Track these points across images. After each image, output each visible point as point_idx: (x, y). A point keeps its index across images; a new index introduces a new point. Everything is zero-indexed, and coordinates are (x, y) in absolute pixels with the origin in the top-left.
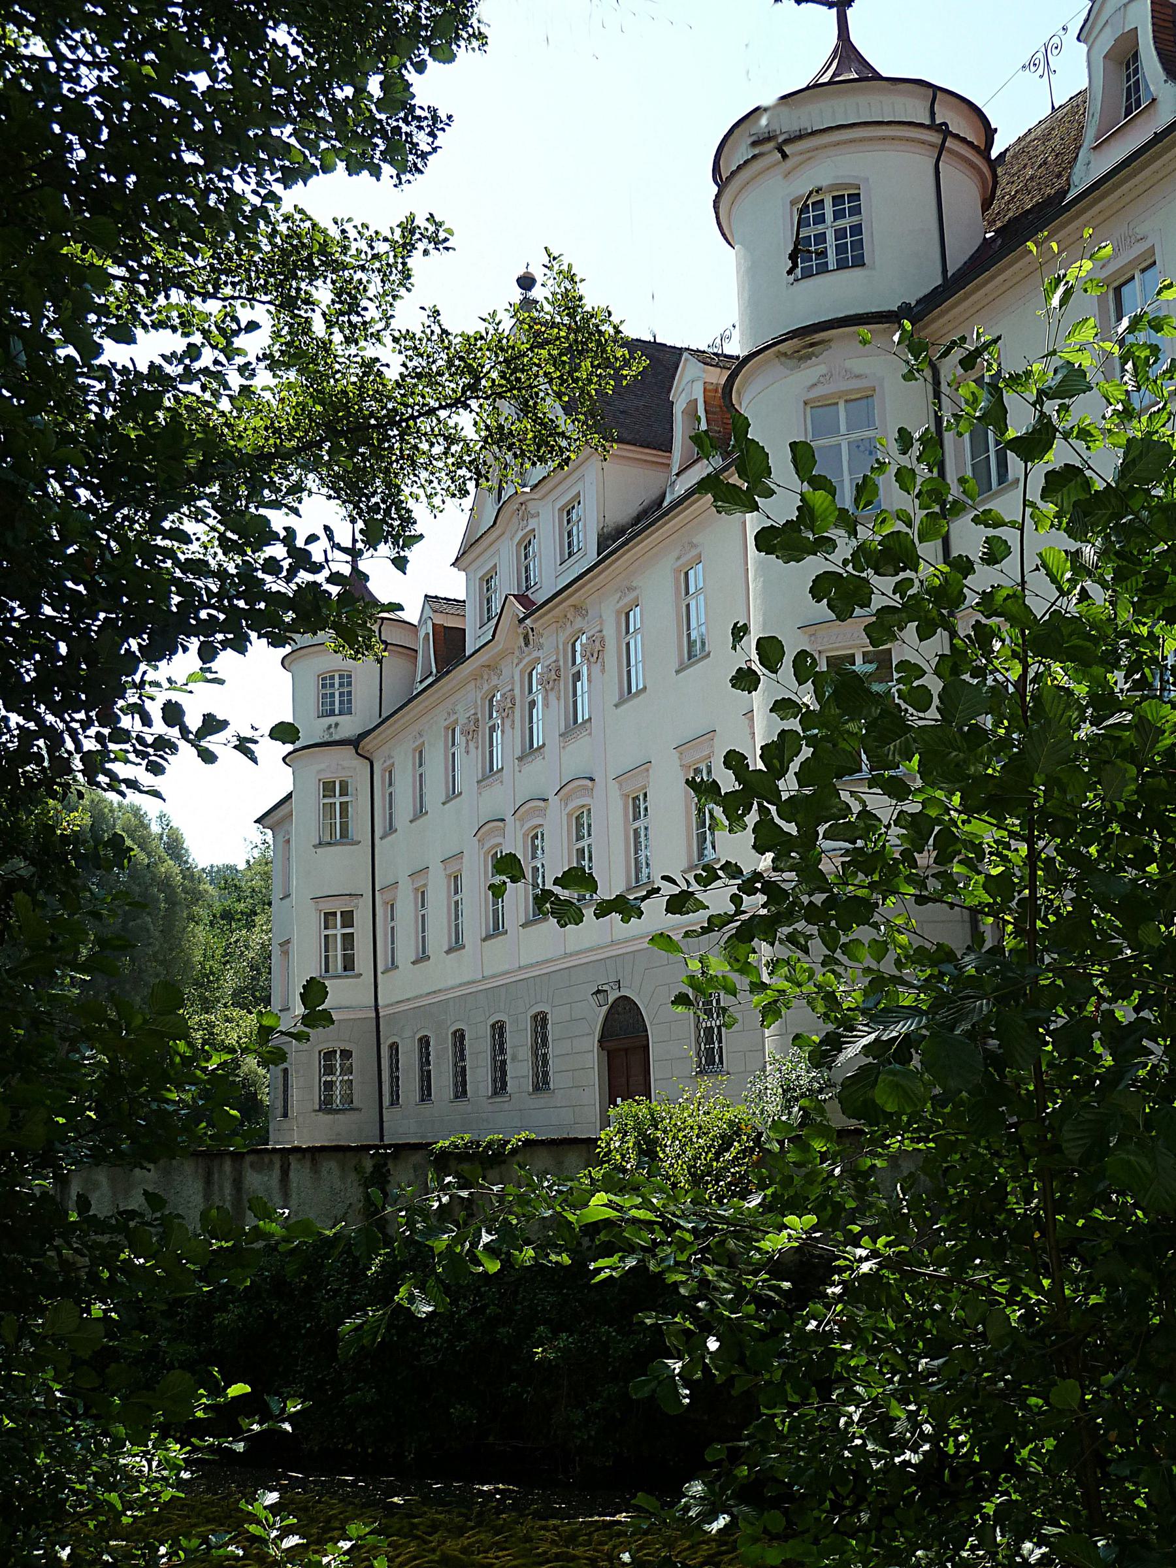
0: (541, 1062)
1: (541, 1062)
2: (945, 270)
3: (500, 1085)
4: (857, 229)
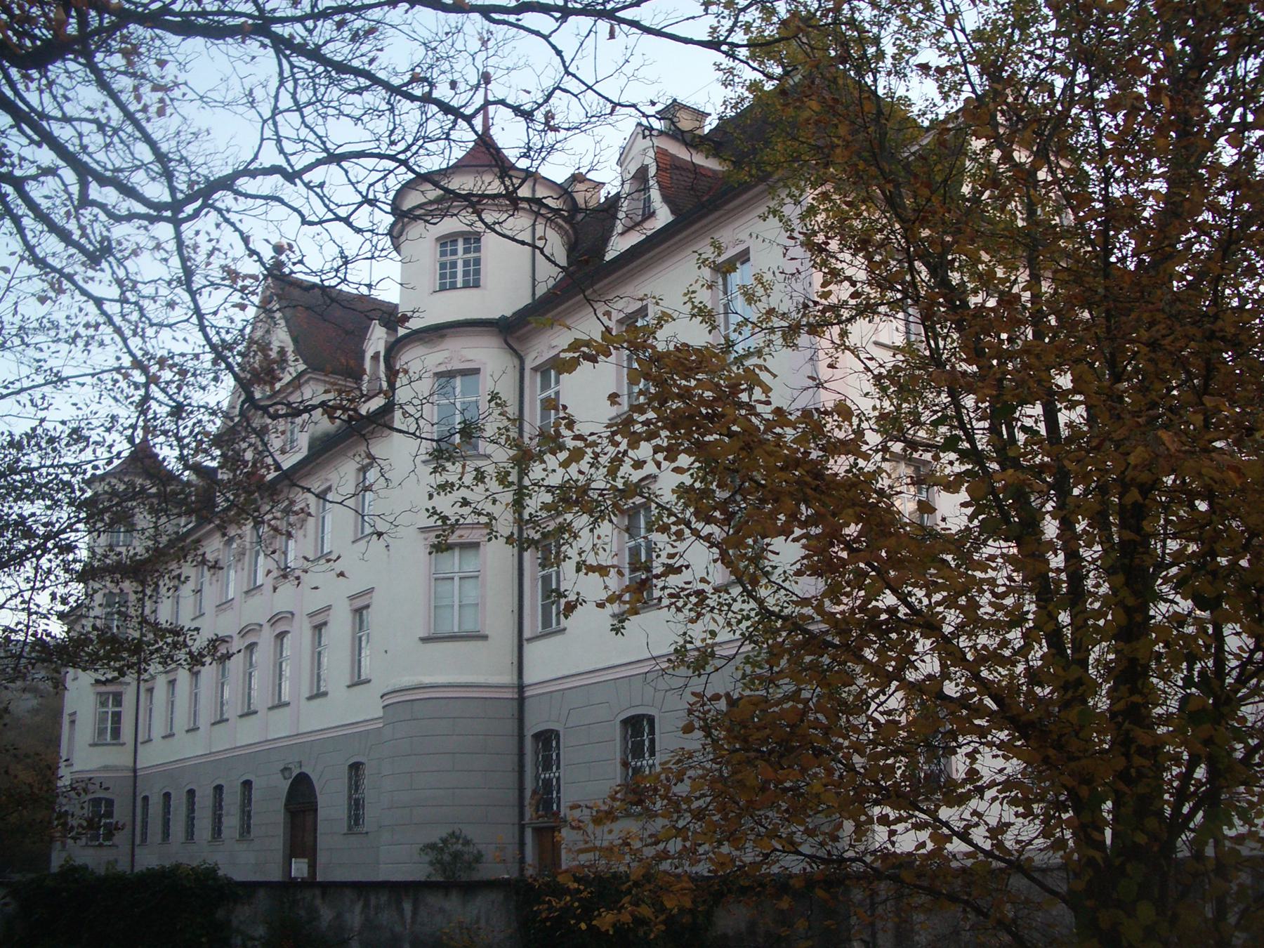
0: (246, 815)
1: (246, 815)
2: (534, 294)
3: (217, 831)
4: (477, 261)
